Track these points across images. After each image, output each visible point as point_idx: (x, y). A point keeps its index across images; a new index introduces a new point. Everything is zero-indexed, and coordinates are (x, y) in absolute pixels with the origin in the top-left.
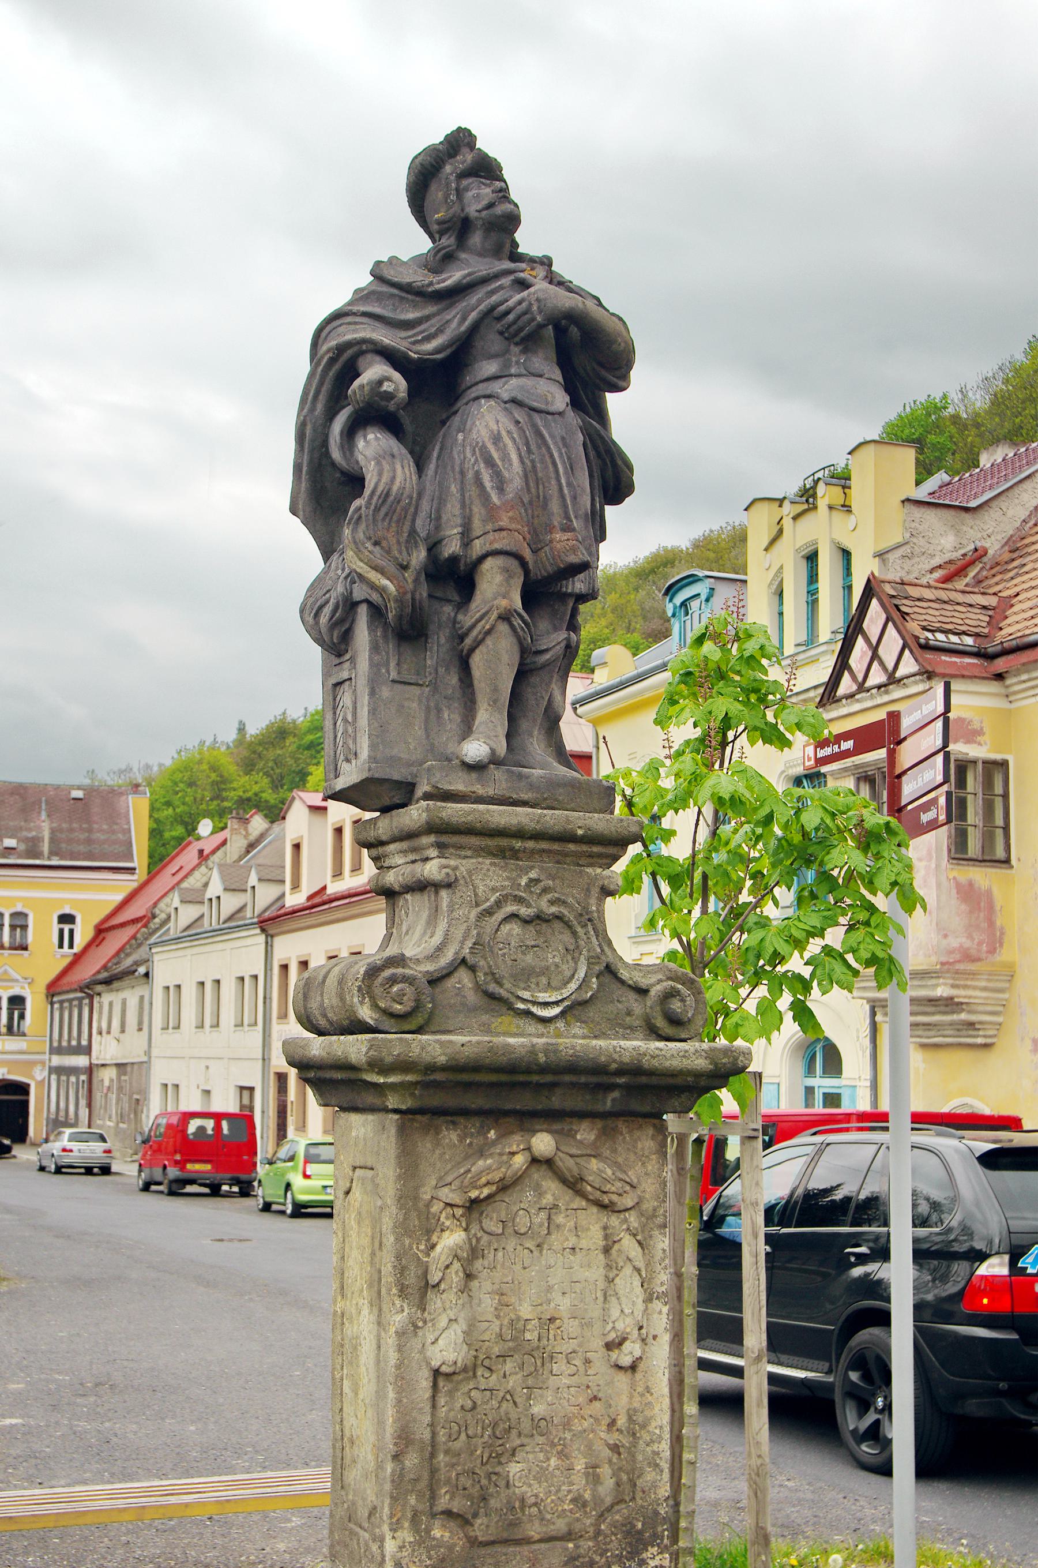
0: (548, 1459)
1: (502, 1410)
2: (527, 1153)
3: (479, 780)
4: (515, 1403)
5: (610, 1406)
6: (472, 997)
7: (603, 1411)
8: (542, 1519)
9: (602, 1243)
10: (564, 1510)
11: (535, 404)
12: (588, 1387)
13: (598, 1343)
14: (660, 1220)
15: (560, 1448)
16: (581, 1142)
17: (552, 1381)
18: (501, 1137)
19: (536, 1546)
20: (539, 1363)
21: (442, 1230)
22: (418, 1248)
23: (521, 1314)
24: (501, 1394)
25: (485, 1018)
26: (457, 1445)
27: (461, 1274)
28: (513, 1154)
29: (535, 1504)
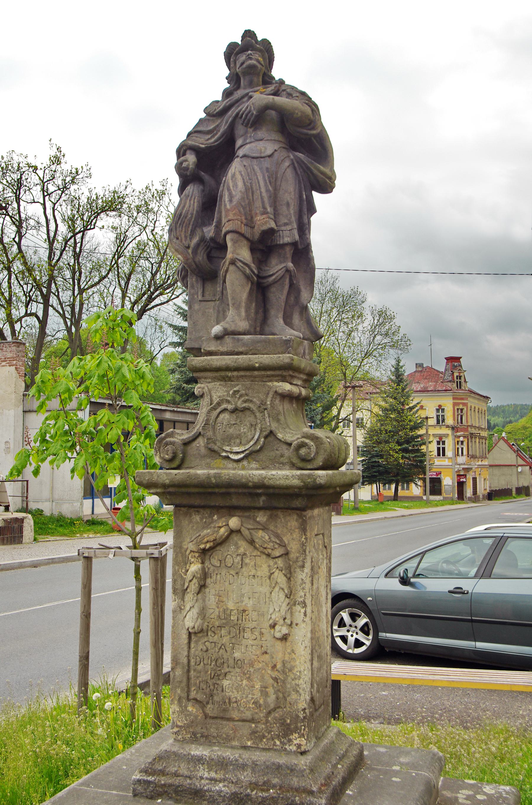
0: (242, 680)
2: (227, 527)
3: (221, 344)
5: (273, 658)
6: (203, 451)
8: (239, 710)
9: (268, 574)
10: (249, 707)
11: (254, 155)
12: (262, 646)
13: (266, 625)
14: (300, 563)
15: (248, 676)
17: (244, 642)
18: (219, 518)
19: (236, 723)
20: (238, 632)
23: (229, 607)
24: (220, 645)
25: (208, 460)
26: (200, 668)
27: (197, 585)
28: (220, 527)
29: (236, 702)
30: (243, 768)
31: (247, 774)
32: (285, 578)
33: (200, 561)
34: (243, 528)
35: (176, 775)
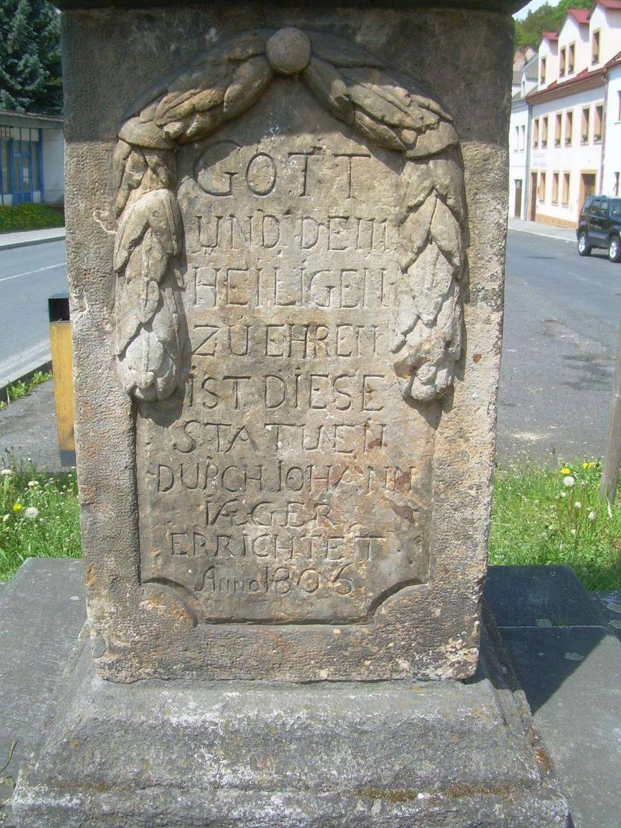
1: (233, 452)
2: (260, 61)
4: (253, 443)
5: (400, 455)
7: (389, 462)
10: (327, 589)
12: (366, 426)
16: (363, 47)
17: (312, 416)
20: (290, 390)
21: (131, 188)
22: (98, 215)
27: (157, 254)
28: (237, 62)
30: (328, 745)
31: (344, 761)
32: (453, 220)
33: (163, 177)
34: (315, 62)
35: (141, 784)
